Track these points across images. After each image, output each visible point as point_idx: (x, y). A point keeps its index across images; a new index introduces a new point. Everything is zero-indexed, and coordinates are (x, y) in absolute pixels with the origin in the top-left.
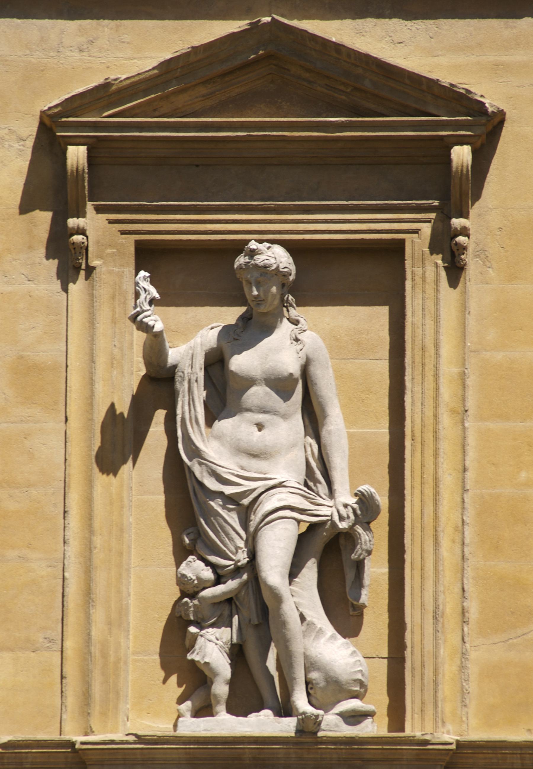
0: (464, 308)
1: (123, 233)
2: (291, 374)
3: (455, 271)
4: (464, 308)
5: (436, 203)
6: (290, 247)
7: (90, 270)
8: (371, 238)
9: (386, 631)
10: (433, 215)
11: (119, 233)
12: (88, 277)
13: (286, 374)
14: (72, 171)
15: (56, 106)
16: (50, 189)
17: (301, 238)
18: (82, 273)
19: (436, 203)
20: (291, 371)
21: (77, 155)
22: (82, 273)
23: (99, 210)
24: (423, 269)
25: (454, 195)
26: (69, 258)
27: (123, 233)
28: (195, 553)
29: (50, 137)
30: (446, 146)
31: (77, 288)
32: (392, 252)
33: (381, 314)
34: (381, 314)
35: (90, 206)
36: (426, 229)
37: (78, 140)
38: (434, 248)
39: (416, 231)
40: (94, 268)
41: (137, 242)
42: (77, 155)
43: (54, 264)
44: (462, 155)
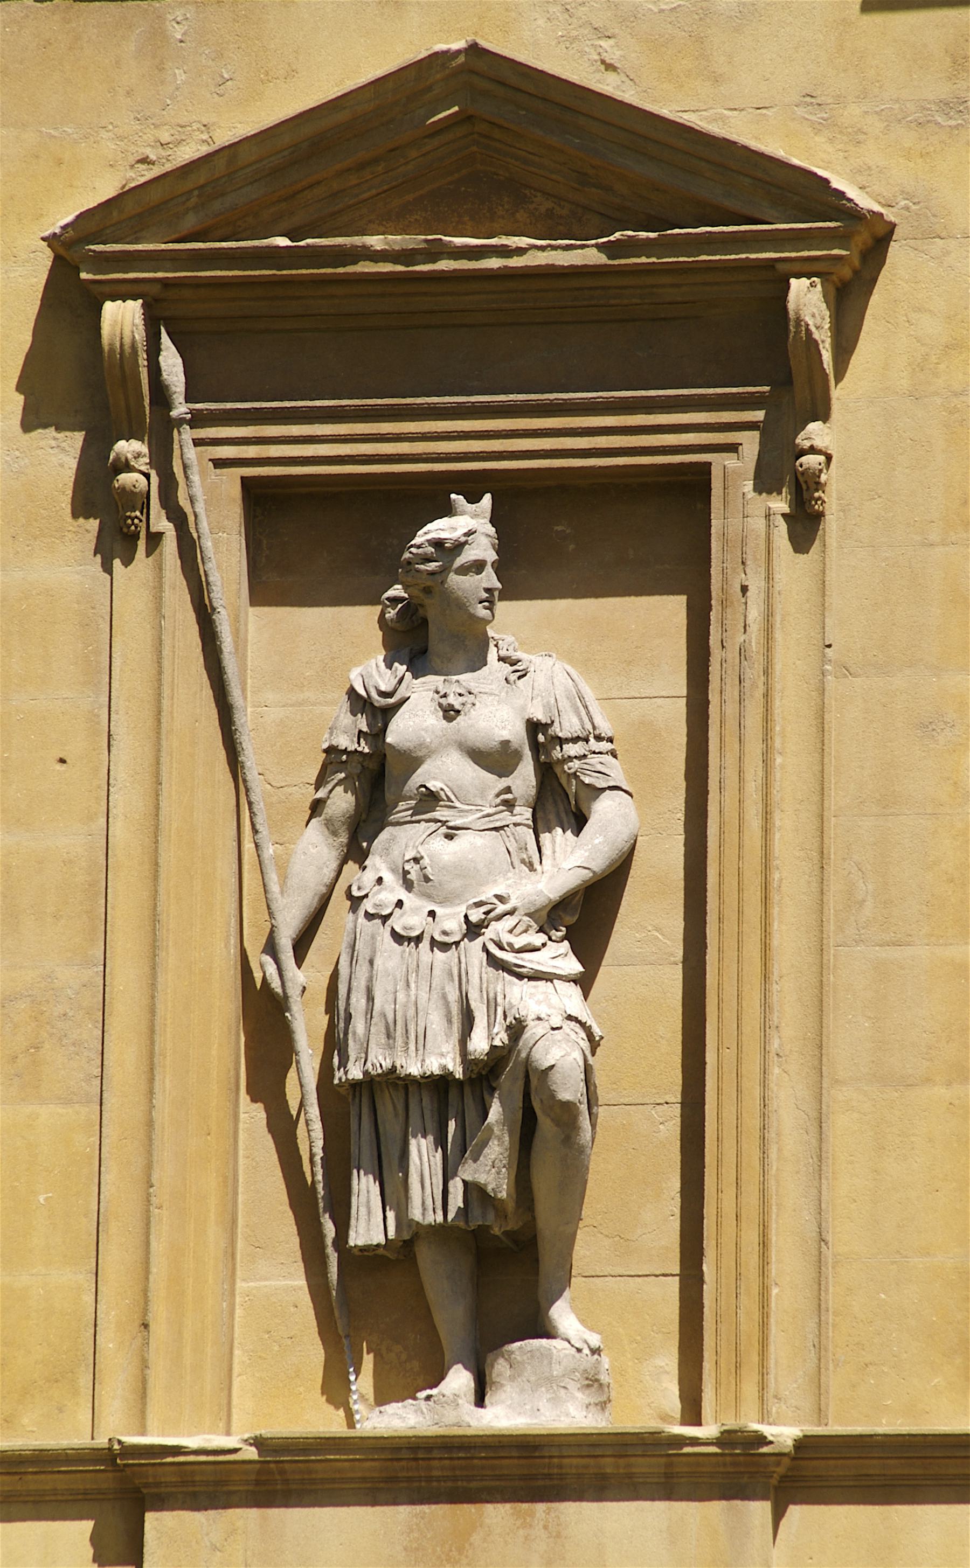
1: (219, 463)
2: (506, 743)
3: (805, 524)
8: (474, 468)
13: (494, 744)
14: (112, 350)
16: (74, 382)
17: (679, 461)
18: (142, 544)
20: (505, 735)
22: (142, 544)
24: (745, 514)
25: (789, 385)
26: (113, 519)
27: (219, 463)
30: (776, 281)
32: (688, 490)
33: (672, 609)
34: (672, 609)
36: (750, 443)
37: (123, 288)
38: (765, 482)
39: (733, 448)
41: (243, 479)
44: (806, 299)
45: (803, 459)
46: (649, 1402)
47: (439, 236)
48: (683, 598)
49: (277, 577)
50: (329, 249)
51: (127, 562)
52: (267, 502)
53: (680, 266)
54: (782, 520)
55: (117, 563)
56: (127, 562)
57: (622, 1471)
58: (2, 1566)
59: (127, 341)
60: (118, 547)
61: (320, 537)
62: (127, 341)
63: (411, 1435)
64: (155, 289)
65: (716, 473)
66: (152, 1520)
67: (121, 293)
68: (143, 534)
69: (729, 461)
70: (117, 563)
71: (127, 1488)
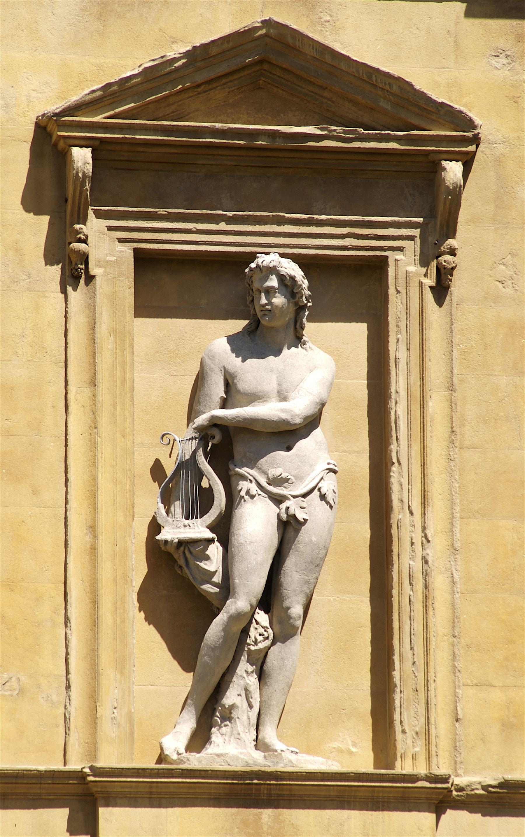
0: (92, 308)
3: (441, 291)
4: (92, 308)
5: (421, 220)
6: (300, 260)
7: (90, 279)
9: (369, 658)
10: (416, 232)
11: (117, 241)
12: (87, 284)
15: (98, 90)
18: (82, 281)
19: (421, 220)
21: (82, 157)
23: (99, 215)
25: (439, 219)
28: (269, 614)
29: (48, 141)
31: (76, 296)
32: (373, 270)
35: (91, 213)
39: (400, 249)
40: (94, 277)
41: (135, 249)
42: (82, 157)
43: (56, 271)
45: (71, 245)
46: (350, 752)
47: (389, 132)
48: (364, 326)
49: (149, 303)
50: (180, 127)
51: (75, 290)
52: (146, 262)
53: (190, 144)
54: (429, 288)
55: (69, 289)
56: (75, 290)
57: (243, 792)
58: (1, 835)
59: (458, 184)
60: (70, 280)
61: (167, 283)
62: (458, 184)
63: (208, 769)
64: (97, 143)
65: (391, 262)
66: (103, 812)
67: (83, 143)
68: (83, 276)
69: (399, 256)
70: (69, 289)
71: (83, 794)
